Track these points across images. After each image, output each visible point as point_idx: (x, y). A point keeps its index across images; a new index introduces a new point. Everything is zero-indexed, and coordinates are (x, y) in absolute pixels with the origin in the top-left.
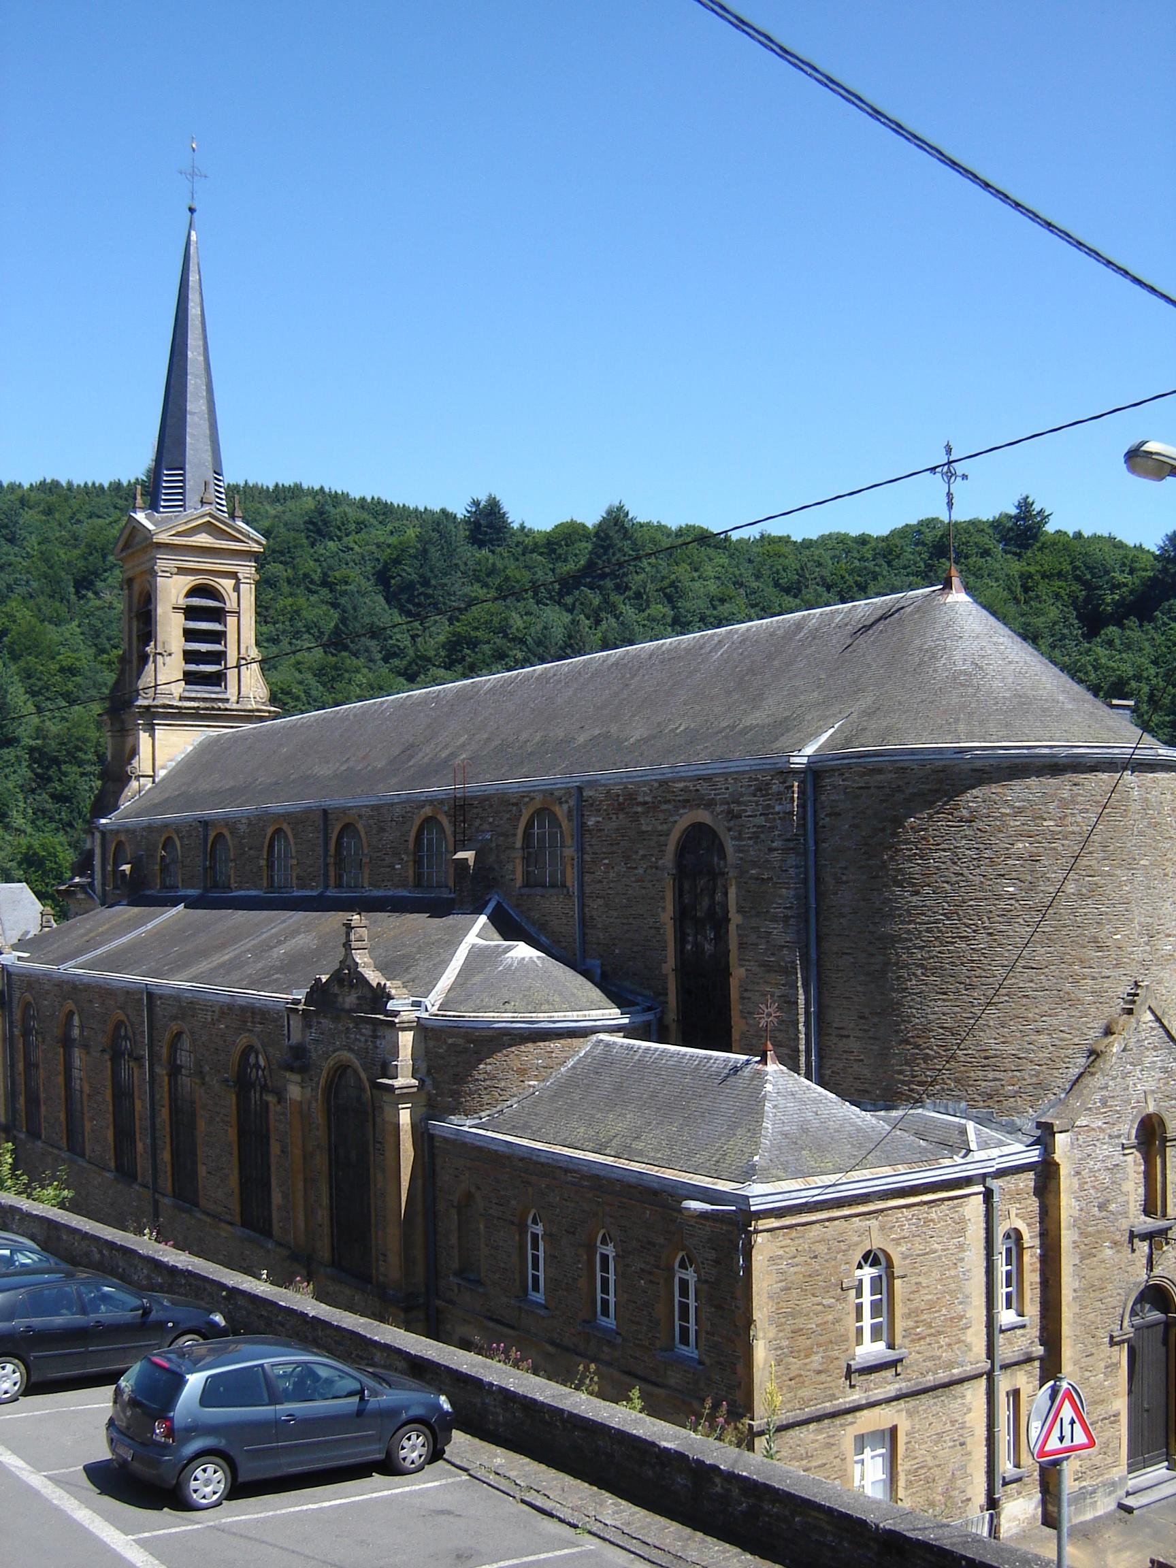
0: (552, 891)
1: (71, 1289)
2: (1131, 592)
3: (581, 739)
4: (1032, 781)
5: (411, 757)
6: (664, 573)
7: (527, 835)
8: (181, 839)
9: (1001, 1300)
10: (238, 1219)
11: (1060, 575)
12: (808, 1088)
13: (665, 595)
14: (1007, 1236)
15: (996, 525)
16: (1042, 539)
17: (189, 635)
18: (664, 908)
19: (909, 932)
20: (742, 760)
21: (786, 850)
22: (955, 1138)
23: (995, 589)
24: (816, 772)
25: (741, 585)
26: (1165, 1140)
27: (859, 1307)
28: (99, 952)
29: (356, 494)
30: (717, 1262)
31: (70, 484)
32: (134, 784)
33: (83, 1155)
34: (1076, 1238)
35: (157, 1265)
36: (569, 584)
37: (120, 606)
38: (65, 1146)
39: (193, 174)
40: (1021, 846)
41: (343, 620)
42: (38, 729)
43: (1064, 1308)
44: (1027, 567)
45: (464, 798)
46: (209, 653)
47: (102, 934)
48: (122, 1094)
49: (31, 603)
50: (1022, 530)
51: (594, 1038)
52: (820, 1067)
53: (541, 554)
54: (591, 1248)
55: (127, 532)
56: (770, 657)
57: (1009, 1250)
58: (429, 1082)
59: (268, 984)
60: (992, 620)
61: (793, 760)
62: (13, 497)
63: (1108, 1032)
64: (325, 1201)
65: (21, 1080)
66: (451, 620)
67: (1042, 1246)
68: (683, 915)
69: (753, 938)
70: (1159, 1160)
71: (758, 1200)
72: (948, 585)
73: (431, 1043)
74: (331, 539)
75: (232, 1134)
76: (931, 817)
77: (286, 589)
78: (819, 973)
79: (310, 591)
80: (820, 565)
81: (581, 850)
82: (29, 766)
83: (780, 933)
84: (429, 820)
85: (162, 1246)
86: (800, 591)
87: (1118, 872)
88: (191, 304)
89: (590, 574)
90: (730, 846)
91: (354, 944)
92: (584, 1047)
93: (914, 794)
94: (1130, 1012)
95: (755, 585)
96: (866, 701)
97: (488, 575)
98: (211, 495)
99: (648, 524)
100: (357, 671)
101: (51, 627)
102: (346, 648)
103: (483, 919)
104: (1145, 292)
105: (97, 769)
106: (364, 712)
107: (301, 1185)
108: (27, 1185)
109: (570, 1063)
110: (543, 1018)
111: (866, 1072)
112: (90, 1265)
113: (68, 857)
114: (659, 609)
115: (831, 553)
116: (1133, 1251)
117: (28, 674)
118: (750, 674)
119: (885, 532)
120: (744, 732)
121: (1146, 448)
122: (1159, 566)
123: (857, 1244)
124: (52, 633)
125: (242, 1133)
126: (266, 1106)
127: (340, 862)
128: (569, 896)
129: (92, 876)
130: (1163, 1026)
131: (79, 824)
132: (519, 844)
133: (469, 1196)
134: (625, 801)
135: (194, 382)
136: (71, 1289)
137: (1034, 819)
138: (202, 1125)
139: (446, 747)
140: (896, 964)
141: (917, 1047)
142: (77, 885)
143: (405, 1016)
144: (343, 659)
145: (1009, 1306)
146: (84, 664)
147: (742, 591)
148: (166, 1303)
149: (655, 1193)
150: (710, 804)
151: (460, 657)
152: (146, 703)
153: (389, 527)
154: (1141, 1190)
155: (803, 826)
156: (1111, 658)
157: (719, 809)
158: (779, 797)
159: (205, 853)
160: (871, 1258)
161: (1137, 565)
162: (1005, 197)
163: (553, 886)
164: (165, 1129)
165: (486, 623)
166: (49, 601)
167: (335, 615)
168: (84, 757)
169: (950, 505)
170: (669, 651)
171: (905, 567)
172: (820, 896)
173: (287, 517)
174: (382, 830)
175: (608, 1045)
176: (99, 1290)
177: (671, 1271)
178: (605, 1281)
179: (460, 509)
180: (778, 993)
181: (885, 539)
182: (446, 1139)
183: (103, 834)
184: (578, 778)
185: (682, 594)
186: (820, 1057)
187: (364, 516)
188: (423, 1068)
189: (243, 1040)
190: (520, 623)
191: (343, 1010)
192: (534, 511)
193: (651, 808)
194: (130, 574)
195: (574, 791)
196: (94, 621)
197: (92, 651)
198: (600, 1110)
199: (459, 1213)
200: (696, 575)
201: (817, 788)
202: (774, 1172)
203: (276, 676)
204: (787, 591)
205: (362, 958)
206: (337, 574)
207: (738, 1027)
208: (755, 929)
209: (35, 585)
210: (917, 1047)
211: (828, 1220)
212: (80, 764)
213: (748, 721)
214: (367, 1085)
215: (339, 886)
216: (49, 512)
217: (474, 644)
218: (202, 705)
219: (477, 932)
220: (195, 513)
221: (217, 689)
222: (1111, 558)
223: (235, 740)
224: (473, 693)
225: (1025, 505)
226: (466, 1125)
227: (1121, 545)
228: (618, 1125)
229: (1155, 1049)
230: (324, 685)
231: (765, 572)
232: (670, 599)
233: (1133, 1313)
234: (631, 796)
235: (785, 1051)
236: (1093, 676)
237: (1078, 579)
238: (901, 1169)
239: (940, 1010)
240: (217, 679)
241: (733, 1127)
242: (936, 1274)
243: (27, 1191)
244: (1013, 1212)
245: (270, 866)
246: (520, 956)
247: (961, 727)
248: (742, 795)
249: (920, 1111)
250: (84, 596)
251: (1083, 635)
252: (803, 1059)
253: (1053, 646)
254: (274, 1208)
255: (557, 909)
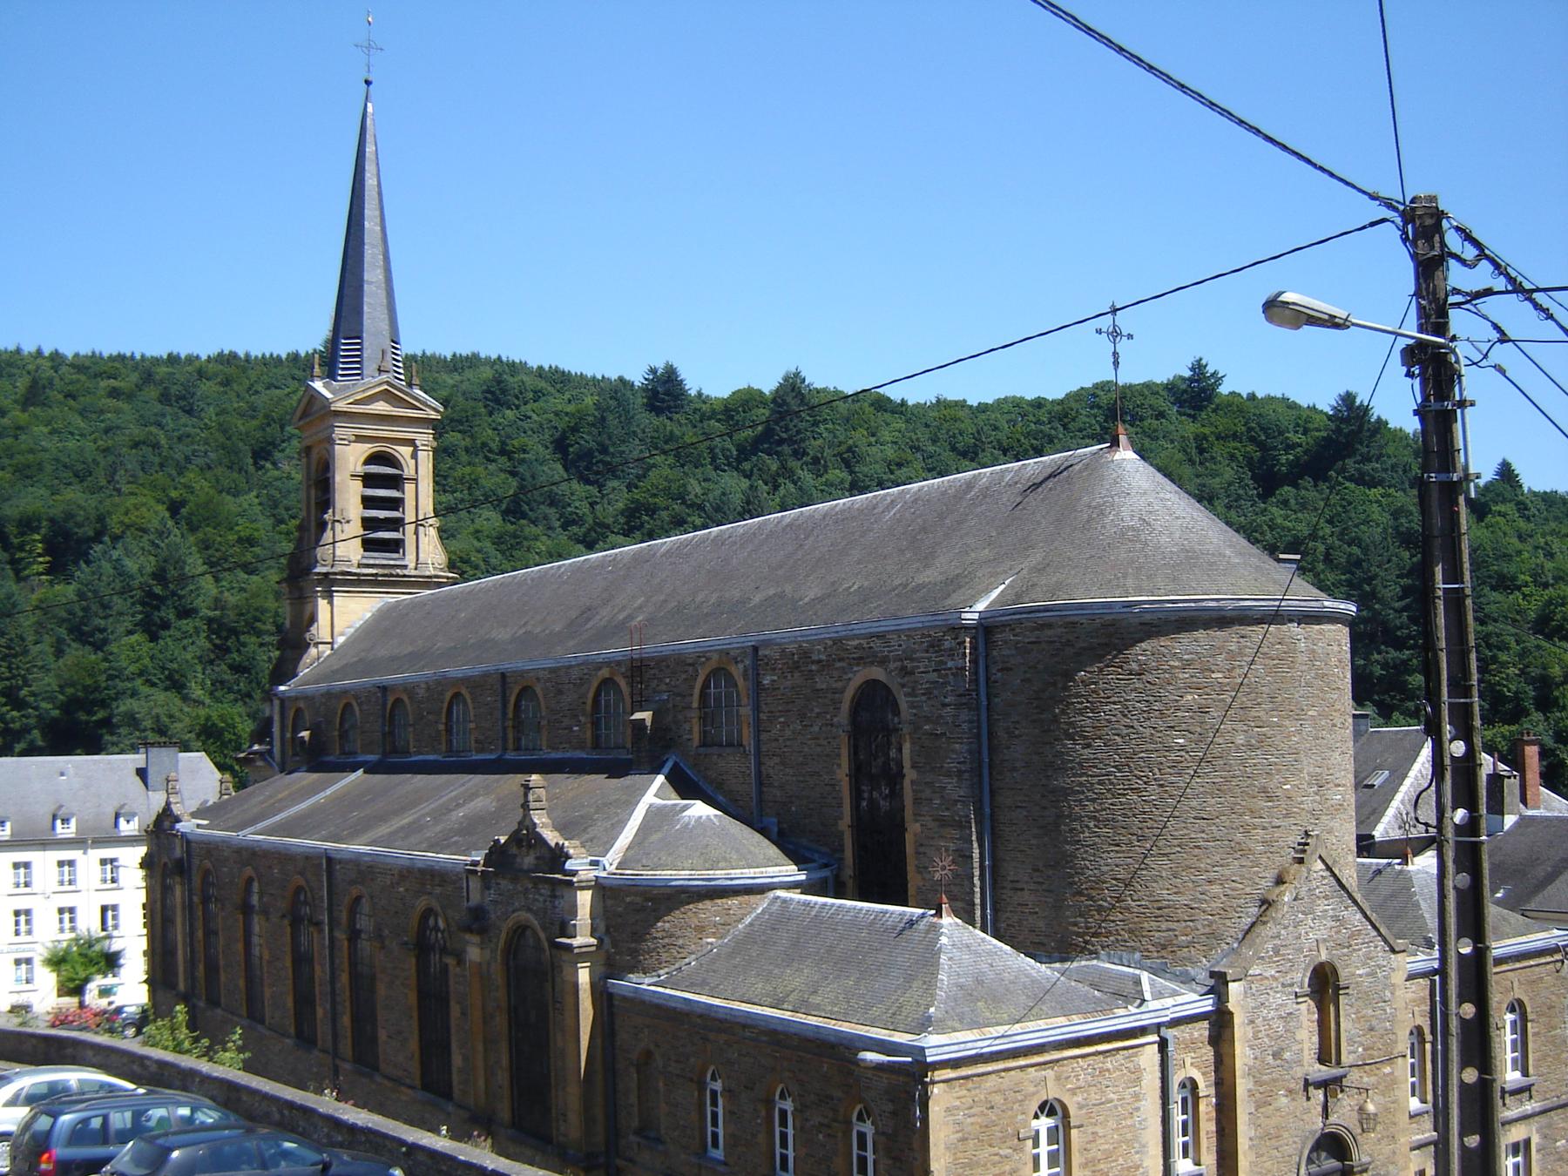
0: (728, 750)
1: (251, 1144)
2: (1305, 452)
3: (757, 599)
4: (1200, 634)
5: (589, 619)
6: (842, 438)
7: (704, 695)
8: (360, 705)
9: (1177, 1150)
10: (418, 1082)
11: (1235, 436)
12: (983, 940)
13: (843, 460)
14: (1183, 1085)
15: (1170, 387)
16: (1217, 400)
17: (368, 502)
18: (839, 766)
19: (1081, 784)
20: (912, 616)
21: (958, 706)
22: (1129, 988)
23: (1169, 450)
24: (987, 628)
25: (918, 449)
26: (1338, 988)
27: (1036, 1158)
28: (278, 818)
29: (533, 363)
30: (894, 1113)
31: (247, 355)
32: (313, 651)
33: (262, 1022)
34: (1251, 1086)
35: (336, 1123)
36: (745, 452)
37: (298, 477)
38: (244, 1013)
39: (369, 47)
40: (1189, 697)
41: (522, 487)
42: (217, 600)
43: (1241, 1157)
44: (1191, 424)
45: (642, 660)
46: (387, 520)
47: (280, 800)
48: (302, 961)
49: (209, 474)
50: (1196, 392)
51: (771, 894)
52: (995, 921)
53: (719, 421)
54: (770, 1103)
55: (305, 400)
56: (942, 517)
57: (1184, 1100)
58: (607, 940)
59: (448, 846)
60: (1159, 476)
61: (964, 616)
62: (189, 369)
63: (1280, 881)
64: (505, 1061)
65: (200, 948)
66: (629, 487)
67: (1217, 1095)
68: (858, 773)
69: (928, 793)
70: (1332, 1009)
71: (934, 1051)
72: (1115, 443)
73: (609, 902)
74: (509, 408)
75: (413, 998)
76: (1101, 670)
77: (464, 458)
78: (993, 828)
79: (488, 459)
80: (996, 428)
81: (757, 709)
82: (208, 637)
83: (954, 788)
84: (607, 683)
85: (342, 1105)
86: (976, 454)
87: (1287, 723)
88: (367, 175)
89: (767, 440)
90: (903, 706)
91: (532, 805)
92: (761, 904)
93: (1084, 649)
94: (1301, 861)
95: (931, 449)
96: (1036, 557)
97: (666, 442)
98: (388, 364)
99: (824, 390)
100: (536, 539)
101: (229, 497)
102: (524, 516)
103: (660, 779)
104: (1277, 150)
105: (274, 639)
106: (542, 576)
107: (480, 1048)
108: (209, 1048)
109: (748, 920)
110: (721, 876)
111: (1041, 924)
112: (271, 1124)
113: (246, 727)
114: (837, 474)
115: (1008, 417)
116: (1308, 1099)
117: (205, 545)
118: (920, 534)
119: (1060, 395)
120: (918, 588)
121: (1284, 298)
122: (1332, 426)
123: (1034, 1094)
124: (230, 504)
125: (423, 995)
126: (445, 969)
127: (518, 726)
128: (745, 755)
129: (271, 743)
130: (1334, 875)
131: (258, 695)
132: (695, 705)
133: (649, 1054)
134: (800, 660)
135: (371, 253)
136: (251, 1144)
137: (1202, 671)
138: (382, 990)
139: (623, 608)
140: (1069, 816)
141: (1091, 898)
142: (255, 753)
143: (583, 875)
144: (522, 527)
145: (1185, 1155)
146: (261, 534)
147: (919, 455)
148: (345, 1158)
149: (833, 1046)
150: (883, 662)
151: (637, 523)
152: (324, 570)
153: (567, 396)
154: (1315, 1039)
155: (975, 681)
156: (1286, 518)
157: (892, 666)
158: (951, 653)
159: (384, 716)
160: (1047, 1108)
161: (1310, 426)
162: (1139, 61)
163: (730, 744)
164: (345, 996)
165: (664, 489)
166: (228, 472)
167: (514, 483)
168: (264, 627)
169: (1116, 364)
170: (842, 511)
171: (1080, 430)
172: (992, 749)
173: (464, 387)
174: (560, 692)
175: (785, 901)
176: (279, 1146)
177: (849, 1123)
178: (784, 1136)
179: (637, 377)
180: (952, 846)
181: (1061, 402)
182: (624, 998)
183: (282, 701)
184: (753, 639)
185: (860, 459)
186: (995, 910)
187: (542, 384)
188: (602, 928)
189: (422, 903)
190: (698, 490)
191: (521, 870)
192: (712, 377)
193: (825, 666)
194: (307, 442)
195: (749, 651)
196: (273, 492)
197: (270, 521)
198: (777, 966)
199: (638, 1072)
200: (873, 439)
201: (989, 643)
202: (950, 1023)
203: (455, 545)
204: (964, 454)
205: (539, 818)
206: (515, 443)
207: (914, 881)
208: (930, 784)
209: (212, 455)
210: (1091, 898)
211: (1005, 1070)
212: (259, 634)
213: (921, 578)
214: (546, 945)
215: (518, 749)
216: (227, 383)
217: (652, 511)
218: (380, 571)
219: (654, 792)
220: (372, 381)
221: (395, 555)
222: (1286, 419)
223: (413, 606)
224: (652, 552)
225: (1198, 367)
226: (644, 983)
227: (1293, 406)
228: (795, 980)
229: (1326, 897)
230: (503, 553)
231: (942, 435)
232: (847, 464)
233: (1310, 1161)
234: (805, 654)
235: (959, 904)
236: (1269, 536)
237: (1253, 440)
238: (1076, 1019)
239: (1112, 863)
240: (396, 546)
241: (910, 979)
242: (1112, 1124)
243: (208, 1054)
244: (1188, 1061)
245: (449, 730)
246: (697, 814)
247: (1130, 582)
248: (915, 651)
249: (1095, 962)
250: (263, 467)
251: (1259, 495)
252: (978, 913)
253: (1229, 507)
254: (454, 1070)
255: (734, 768)
